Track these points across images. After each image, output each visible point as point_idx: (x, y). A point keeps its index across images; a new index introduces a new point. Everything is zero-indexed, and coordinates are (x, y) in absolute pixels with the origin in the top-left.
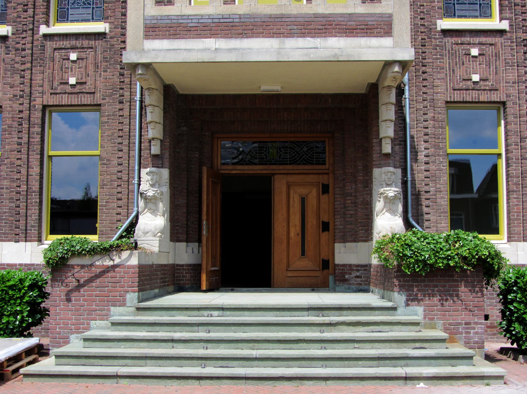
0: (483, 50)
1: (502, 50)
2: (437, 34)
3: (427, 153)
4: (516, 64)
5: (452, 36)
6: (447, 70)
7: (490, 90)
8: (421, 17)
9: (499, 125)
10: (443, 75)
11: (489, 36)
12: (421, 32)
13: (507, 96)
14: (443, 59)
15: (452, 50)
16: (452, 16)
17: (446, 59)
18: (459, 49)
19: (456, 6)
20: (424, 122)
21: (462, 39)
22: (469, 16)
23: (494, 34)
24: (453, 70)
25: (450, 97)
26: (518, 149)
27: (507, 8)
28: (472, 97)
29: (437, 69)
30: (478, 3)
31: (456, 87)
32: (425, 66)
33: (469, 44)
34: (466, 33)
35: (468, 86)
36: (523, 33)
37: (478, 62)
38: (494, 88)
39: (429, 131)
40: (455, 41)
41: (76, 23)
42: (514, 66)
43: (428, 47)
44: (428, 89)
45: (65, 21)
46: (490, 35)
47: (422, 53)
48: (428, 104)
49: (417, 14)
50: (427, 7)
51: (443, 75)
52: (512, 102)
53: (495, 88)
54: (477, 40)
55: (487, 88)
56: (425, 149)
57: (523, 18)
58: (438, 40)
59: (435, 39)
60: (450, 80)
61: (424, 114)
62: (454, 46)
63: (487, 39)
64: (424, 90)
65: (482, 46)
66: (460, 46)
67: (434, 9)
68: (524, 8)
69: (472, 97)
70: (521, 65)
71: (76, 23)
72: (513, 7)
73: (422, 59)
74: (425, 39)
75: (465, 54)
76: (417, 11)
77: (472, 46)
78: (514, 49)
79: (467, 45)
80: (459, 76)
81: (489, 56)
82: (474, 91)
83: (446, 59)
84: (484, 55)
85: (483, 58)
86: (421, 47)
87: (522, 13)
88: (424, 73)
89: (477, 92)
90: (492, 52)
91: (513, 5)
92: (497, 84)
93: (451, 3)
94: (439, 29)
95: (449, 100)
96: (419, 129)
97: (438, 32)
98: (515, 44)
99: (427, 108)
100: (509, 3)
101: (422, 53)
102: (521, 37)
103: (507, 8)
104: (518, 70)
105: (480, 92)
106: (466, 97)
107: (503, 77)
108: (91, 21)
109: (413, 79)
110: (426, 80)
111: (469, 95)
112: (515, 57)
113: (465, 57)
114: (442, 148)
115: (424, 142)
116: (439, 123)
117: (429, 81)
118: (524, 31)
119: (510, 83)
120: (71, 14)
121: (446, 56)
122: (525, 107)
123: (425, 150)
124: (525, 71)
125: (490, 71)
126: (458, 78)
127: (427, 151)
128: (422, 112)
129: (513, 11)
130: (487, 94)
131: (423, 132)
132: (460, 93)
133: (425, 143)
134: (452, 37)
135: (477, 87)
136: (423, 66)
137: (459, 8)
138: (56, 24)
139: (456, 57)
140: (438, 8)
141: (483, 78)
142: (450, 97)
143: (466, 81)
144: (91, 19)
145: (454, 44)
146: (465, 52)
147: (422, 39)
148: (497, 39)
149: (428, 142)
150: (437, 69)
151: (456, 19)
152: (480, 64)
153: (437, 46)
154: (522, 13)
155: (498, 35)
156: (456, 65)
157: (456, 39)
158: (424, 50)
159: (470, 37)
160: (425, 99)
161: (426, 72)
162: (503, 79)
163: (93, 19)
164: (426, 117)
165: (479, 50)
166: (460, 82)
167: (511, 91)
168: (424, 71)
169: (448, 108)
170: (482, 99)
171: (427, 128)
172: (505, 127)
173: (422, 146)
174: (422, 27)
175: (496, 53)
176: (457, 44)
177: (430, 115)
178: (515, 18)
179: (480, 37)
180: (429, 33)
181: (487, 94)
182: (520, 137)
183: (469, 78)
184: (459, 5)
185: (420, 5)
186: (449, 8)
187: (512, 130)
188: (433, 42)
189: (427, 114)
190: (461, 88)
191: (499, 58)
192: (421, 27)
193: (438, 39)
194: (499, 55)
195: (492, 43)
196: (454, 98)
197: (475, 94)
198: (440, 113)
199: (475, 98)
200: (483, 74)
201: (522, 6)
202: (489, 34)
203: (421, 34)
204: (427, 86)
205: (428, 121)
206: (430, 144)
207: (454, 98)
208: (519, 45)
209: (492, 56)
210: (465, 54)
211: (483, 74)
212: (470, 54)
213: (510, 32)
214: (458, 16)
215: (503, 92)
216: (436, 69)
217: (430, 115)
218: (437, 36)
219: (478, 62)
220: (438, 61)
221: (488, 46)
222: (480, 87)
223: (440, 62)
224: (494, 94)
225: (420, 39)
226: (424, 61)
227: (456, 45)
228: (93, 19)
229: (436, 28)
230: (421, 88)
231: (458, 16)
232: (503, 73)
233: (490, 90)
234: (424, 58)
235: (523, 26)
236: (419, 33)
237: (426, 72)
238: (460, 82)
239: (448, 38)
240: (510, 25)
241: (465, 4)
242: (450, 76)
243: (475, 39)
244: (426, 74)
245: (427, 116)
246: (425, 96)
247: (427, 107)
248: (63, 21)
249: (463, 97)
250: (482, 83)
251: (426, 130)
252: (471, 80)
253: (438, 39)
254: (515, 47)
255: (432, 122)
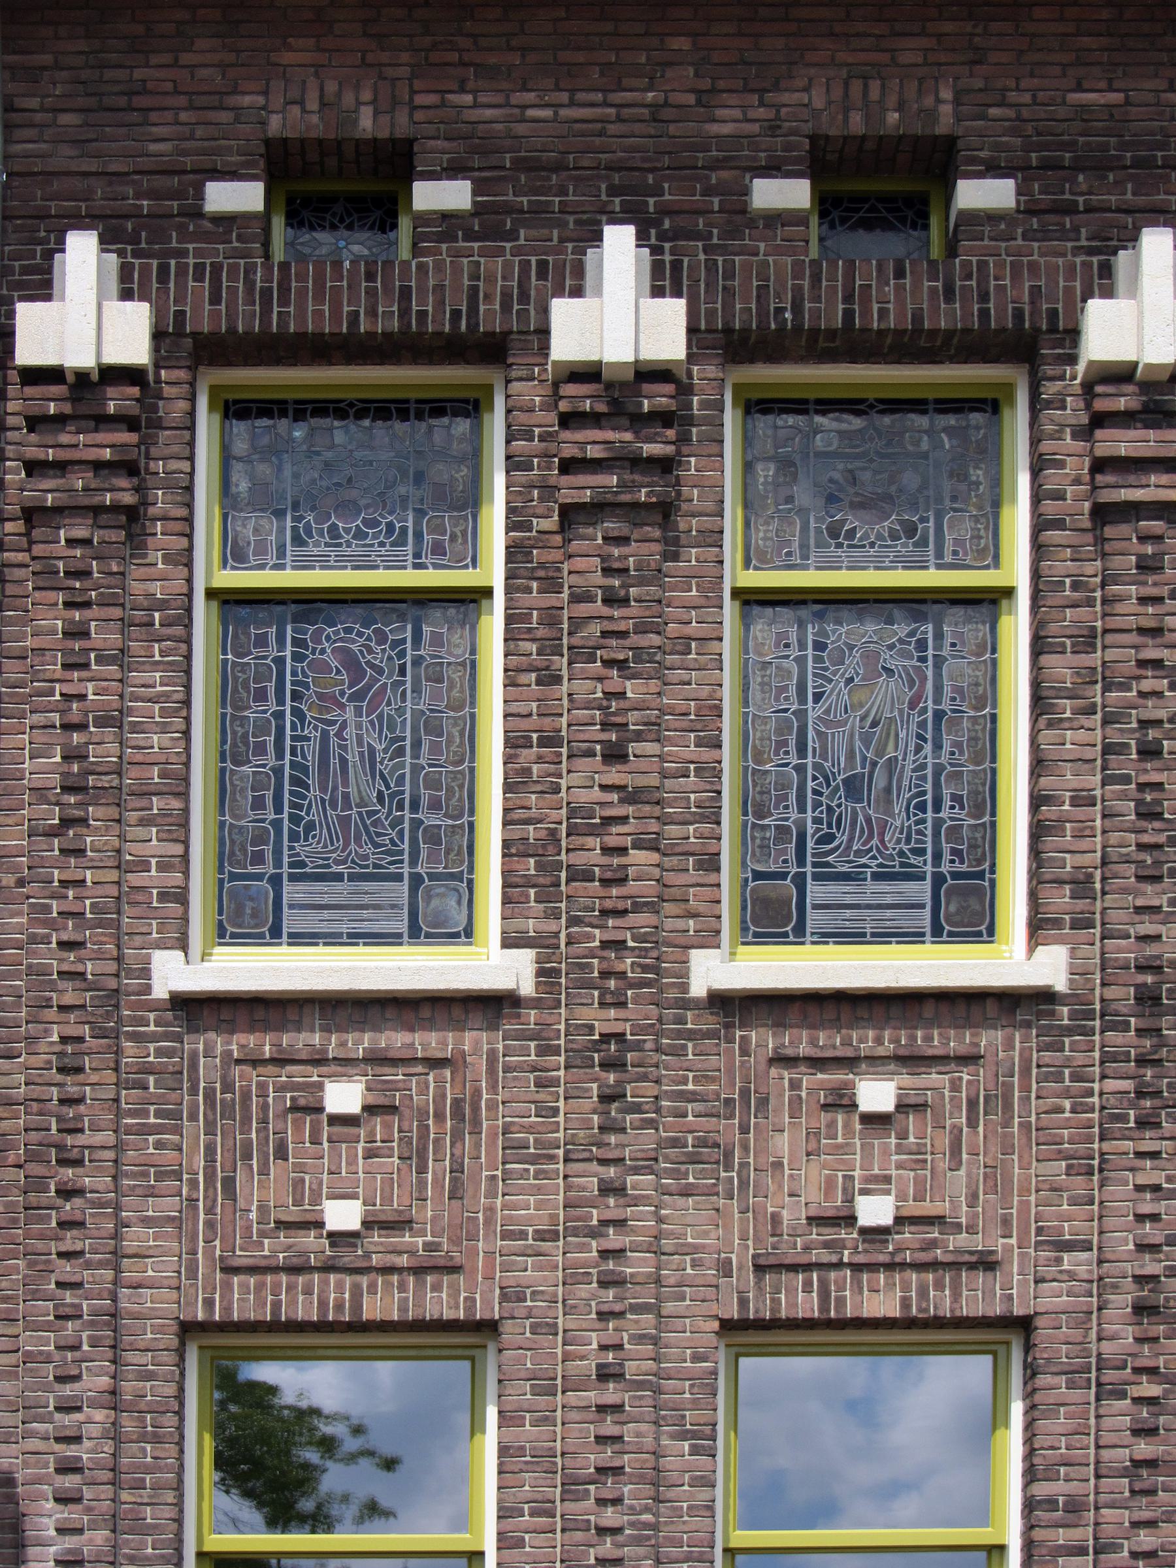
0: (392, 1087)
1: (493, 1088)
2: (152, 1016)
3: (70, 1551)
4: (561, 1152)
5: (230, 1028)
6: (194, 1184)
7: (419, 1271)
8: (65, 937)
9: (476, 1426)
10: (169, 1206)
11: (429, 1025)
12: (62, 1008)
13: (504, 1297)
14: (177, 1130)
15: (228, 1087)
16: (261, 936)
17: (194, 1133)
18: (262, 1086)
19: (287, 887)
20: (57, 1416)
21: (285, 1040)
22: (350, 936)
23: (457, 1012)
24: (229, 1183)
25: (209, 1303)
26: (553, 1531)
27: (532, 891)
28: (323, 1304)
29: (145, 1175)
30: (406, 870)
31: (242, 1257)
32: (78, 1163)
33: (319, 1061)
34: (307, 1010)
35: (304, 1254)
36: (602, 1004)
37: (361, 1145)
38: (439, 1258)
39: (83, 1453)
40: (242, 1047)
41: (321, 949)
42: (552, 1158)
43: (94, 1078)
44: (88, 1265)
45: (786, 935)
46: (431, 1020)
47: (62, 1101)
48: (85, 1335)
49: (47, 923)
50: (100, 890)
51: (169, 1206)
52: (528, 1323)
53: (442, 1262)
54: (361, 1042)
55: (403, 1261)
56: (60, 1531)
57: (606, 937)
58: (152, 1047)
59: (136, 1037)
60: (210, 1225)
61: (61, 1379)
62: (237, 1070)
63: (417, 1038)
64: (66, 1269)
65: (387, 1070)
66: (271, 1069)
67: (140, 898)
68: (614, 892)
69: (323, 1304)
70: (586, 1155)
71: (894, 947)
72: (563, 888)
73: (59, 1131)
74: (80, 1039)
75: (295, 1108)
76: (47, 909)
77: (334, 1068)
78: (555, 1082)
79: (310, 1068)
80: (259, 1208)
81: (423, 1114)
82: (332, 1277)
83: (194, 1133)
84: (392, 1109)
85: (387, 1126)
86: (59, 1078)
87: (605, 913)
88: (67, 1193)
89: (348, 1280)
90: (440, 1097)
91: (563, 875)
92: (455, 1241)
93: (259, 877)
94: (160, 991)
95: (200, 1316)
96: (34, 1444)
97: (155, 1006)
98: (562, 1059)
99: (77, 1354)
100: (539, 866)
101: (62, 1101)
102: (591, 1028)
103: (532, 891)
104: (566, 1177)
105: (364, 1281)
106: (293, 1302)
107: (491, 1210)
108: (928, 938)
109: (15, 1221)
110: (81, 1224)
111: (308, 1292)
112: (561, 1119)
113: (294, 1121)
114: (156, 1526)
115: (57, 1500)
116: (143, 1420)
117: (95, 1233)
118: (609, 999)
119: (523, 1235)
120: (815, 907)
121: (193, 1117)
122: (595, 1346)
123: (60, 1538)
124: (601, 1181)
125: (422, 1184)
126: (253, 1215)
127: (70, 1542)
128: (50, 1371)
129: (563, 905)
130: (402, 1288)
131: (51, 1458)
132: (260, 1287)
133: (61, 1507)
134: (232, 1032)
135: (348, 1258)
136: (62, 1162)
137: (300, 898)
138: (742, 949)
139: (246, 1120)
140: (163, 897)
141: (383, 1217)
142: (209, 1303)
143: (292, 1232)
144: (928, 930)
145: (238, 1062)
146: (293, 1099)
147: (64, 1040)
148: (469, 1036)
149: (78, 1500)
150: (145, 1175)
151: (285, 949)
152: (369, 1154)
153: (148, 1070)
154: (605, 913)
155: (476, 1018)
156: (247, 1156)
157: (251, 1040)
158: (73, 1090)
159: (326, 1029)
160: (69, 1311)
161: (79, 1192)
162: (488, 1222)
163: (937, 931)
164: (68, 1390)
165: (368, 1089)
166: (262, 1234)
167: (530, 1274)
168: (69, 1186)
169: (735, 1349)
170: (372, 1309)
171: (77, 1439)
172: (1029, 1426)
173: (45, 1520)
174: (68, 985)
175: (457, 1103)
176: (255, 1063)
177: (95, 1381)
178: (568, 935)
179: (377, 1029)
180: (101, 1011)
181: (402, 1288)
182: (1096, 1469)
183: (309, 1217)
184: (301, 886)
185: (64, 883)
186: (251, 899)
187: (523, 1448)
188: (130, 1052)
189: (77, 1378)
190: (263, 1263)
191: (476, 1122)
192: (62, 985)
193: (154, 1038)
194: (476, 1108)
195: (440, 1055)
196: (227, 1309)
197: (340, 1287)
198: (150, 1376)
199: (339, 1307)
200: (387, 1199)
201: (606, 882)
202: (426, 1012)
203: (63, 1017)
204: (81, 1253)
205: (79, 1409)
206: (88, 1510)
207: (227, 1309)
208: (578, 1062)
209: (439, 1116)
210: (295, 1108)
211: (387, 1199)
212: (321, 1110)
213: (535, 1003)
214: (290, 935)
215: (489, 1278)
216: (133, 1176)
217: (95, 1381)
218: (152, 1028)
219: (361, 1145)
220: (151, 1138)
221: (419, 1069)
222: (367, 1255)
223: (159, 1145)
224: (436, 1288)
225: (55, 1038)
226: (69, 1140)
227: (247, 1069)
228: (937, 931)
229: (148, 989)
230: (48, 1262)
231: (290, 935)
232: (491, 1194)
233: (419, 1271)
234: (71, 1126)
235: (605, 974)
236: (51, 1014)
237: (79, 1192)
238: (262, 1234)
239: (212, 1035)
240: (540, 973)
241: (338, 877)
242: (210, 1211)
243: (350, 1038)
244: (77, 1202)
245: (77, 1386)
246: (69, 1297)
247: (76, 1347)
248: (780, 938)
249: (276, 1305)
250: (376, 1238)
251: (71, 1451)
252: (320, 1225)
253: (154, 1038)
254: (562, 1073)
255: (99, 1415)
